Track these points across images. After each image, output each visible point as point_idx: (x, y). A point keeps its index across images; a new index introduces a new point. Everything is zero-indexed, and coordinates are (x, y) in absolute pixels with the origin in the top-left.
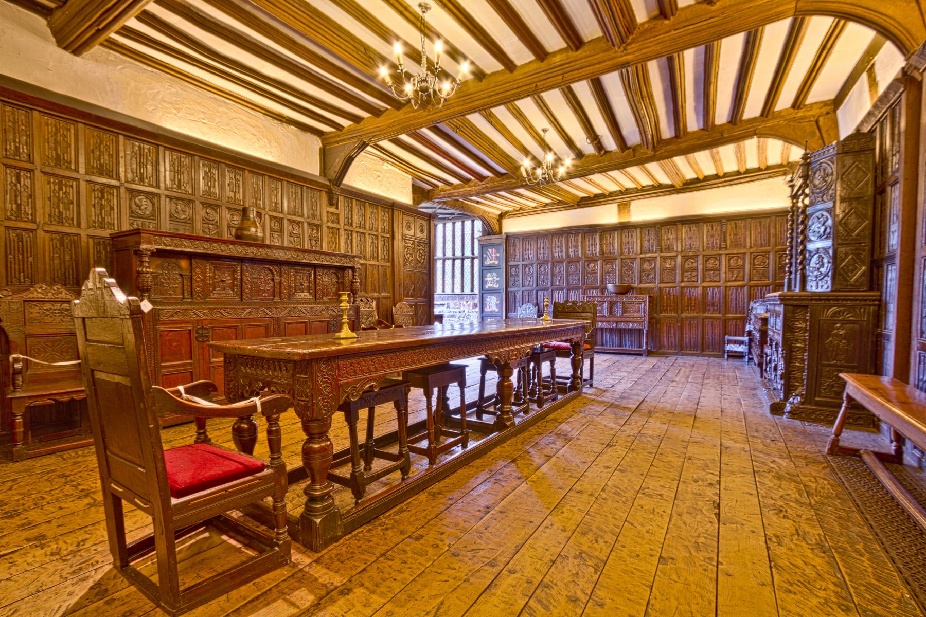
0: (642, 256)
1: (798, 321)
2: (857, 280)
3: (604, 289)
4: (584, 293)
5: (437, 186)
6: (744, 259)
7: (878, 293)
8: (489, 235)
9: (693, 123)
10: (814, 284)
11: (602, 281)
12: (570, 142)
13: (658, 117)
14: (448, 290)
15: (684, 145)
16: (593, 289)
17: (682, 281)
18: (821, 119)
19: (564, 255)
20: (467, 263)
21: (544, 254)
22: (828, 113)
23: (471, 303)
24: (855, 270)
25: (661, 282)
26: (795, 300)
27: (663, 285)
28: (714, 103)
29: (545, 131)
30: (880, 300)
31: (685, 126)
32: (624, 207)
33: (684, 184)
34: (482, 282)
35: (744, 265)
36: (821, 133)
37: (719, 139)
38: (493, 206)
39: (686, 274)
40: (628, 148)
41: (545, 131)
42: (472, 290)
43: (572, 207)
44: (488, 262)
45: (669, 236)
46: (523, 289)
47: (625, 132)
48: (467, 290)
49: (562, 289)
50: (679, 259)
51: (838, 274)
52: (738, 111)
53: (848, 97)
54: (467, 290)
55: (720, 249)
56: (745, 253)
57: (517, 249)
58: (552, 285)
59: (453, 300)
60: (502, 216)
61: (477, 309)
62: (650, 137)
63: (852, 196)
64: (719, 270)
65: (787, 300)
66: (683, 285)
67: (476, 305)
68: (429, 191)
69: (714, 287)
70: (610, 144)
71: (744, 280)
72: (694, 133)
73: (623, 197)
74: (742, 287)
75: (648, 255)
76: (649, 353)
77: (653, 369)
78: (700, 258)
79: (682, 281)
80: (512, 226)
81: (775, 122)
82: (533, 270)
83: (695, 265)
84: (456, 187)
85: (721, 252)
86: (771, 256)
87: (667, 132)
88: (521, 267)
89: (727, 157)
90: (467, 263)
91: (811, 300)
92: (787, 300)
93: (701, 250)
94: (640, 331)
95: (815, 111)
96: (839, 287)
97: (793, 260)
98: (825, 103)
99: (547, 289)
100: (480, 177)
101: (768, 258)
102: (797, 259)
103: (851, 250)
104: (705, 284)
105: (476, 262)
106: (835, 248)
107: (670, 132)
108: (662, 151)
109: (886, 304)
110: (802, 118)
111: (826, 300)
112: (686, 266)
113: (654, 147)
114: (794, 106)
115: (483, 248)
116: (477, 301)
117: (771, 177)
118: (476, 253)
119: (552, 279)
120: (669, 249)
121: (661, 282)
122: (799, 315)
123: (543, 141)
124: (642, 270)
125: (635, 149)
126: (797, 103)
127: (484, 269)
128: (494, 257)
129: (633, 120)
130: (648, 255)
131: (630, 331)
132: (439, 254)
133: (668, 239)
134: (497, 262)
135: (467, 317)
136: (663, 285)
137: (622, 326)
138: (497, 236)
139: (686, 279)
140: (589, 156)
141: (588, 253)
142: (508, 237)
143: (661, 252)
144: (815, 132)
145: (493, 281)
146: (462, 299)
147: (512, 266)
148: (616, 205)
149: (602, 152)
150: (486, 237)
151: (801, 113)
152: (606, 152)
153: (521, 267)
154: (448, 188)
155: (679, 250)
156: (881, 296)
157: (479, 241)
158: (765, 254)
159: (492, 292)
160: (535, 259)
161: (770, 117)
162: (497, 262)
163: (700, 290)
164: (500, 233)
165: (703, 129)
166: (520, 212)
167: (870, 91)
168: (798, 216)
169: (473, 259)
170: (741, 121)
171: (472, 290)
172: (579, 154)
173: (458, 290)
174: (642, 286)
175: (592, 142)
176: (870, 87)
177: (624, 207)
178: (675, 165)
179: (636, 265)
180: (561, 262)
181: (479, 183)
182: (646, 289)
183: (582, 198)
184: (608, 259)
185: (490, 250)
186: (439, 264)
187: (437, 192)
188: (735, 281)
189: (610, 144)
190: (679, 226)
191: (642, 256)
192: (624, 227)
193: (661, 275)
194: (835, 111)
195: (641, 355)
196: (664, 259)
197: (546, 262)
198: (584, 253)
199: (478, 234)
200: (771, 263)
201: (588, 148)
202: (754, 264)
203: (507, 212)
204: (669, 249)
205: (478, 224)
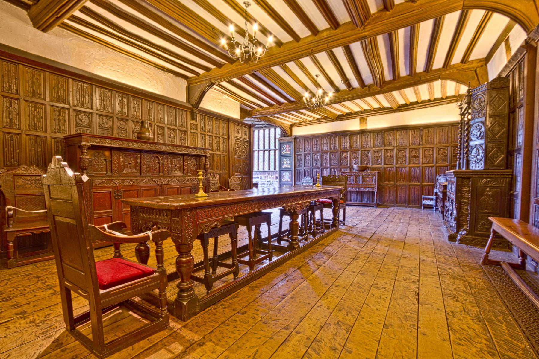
0: (374, 149)
1: (464, 187)
2: (499, 163)
3: (351, 168)
4: (340, 171)
5: (255, 108)
6: (433, 151)
7: (511, 171)
8: (285, 136)
9: (403, 71)
10: (474, 165)
11: (350, 164)
12: (332, 83)
13: (383, 68)
14: (261, 169)
15: (398, 85)
16: (345, 168)
17: (397, 164)
18: (478, 69)
19: (328, 148)
20: (272, 153)
21: (317, 148)
22: (482, 66)
23: (274, 176)
24: (498, 157)
25: (385, 164)
26: (463, 174)
27: (386, 166)
28: (416, 60)
29: (317, 76)
30: (512, 175)
31: (399, 74)
32: (363, 120)
33: (398, 107)
34: (281, 164)
35: (433, 154)
36: (478, 78)
37: (419, 81)
38: (287, 120)
39: (399, 159)
40: (366, 86)
41: (317, 76)
42: (275, 169)
43: (333, 120)
44: (284, 153)
45: (389, 137)
46: (305, 168)
47: (364, 77)
48: (272, 169)
49: (327, 168)
50: (395, 151)
51: (488, 159)
52: (429, 65)
53: (493, 57)
54: (272, 169)
55: (419, 145)
56: (433, 147)
57: (301, 145)
58: (321, 166)
59: (264, 174)
60: (292, 126)
61: (278, 180)
62: (378, 80)
63: (496, 114)
64: (419, 157)
65: (458, 174)
66: (397, 166)
67: (277, 178)
68: (250, 111)
69: (415, 167)
70: (355, 84)
71: (433, 163)
72: (404, 77)
73: (363, 115)
74: (432, 167)
75: (377, 148)
76: (378, 206)
77: (380, 215)
78: (408, 150)
79: (397, 164)
80: (298, 132)
81: (451, 71)
82: (310, 157)
83: (404, 154)
84: (265, 109)
85: (419, 147)
86: (449, 149)
87: (388, 77)
88: (303, 155)
89: (423, 92)
90: (272, 153)
91: (472, 175)
92: (458, 174)
93: (408, 145)
94: (373, 193)
95: (474, 65)
96: (488, 167)
97: (462, 151)
98: (480, 60)
99: (318, 168)
100: (280, 103)
101: (447, 150)
102: (464, 151)
103: (496, 146)
104: (410, 165)
105: (277, 152)
106: (486, 144)
107: (390, 77)
108: (385, 88)
109: (516, 177)
110: (467, 69)
111: (481, 174)
112: (400, 155)
113: (381, 85)
114: (462, 62)
115: (281, 144)
116: (277, 175)
117: (449, 103)
118: (277, 147)
119: (322, 162)
120: (389, 145)
121: (385, 164)
122: (465, 183)
123: (316, 82)
124: (374, 157)
125: (369, 86)
126: (464, 60)
127: (282, 157)
128: (287, 150)
129: (368, 70)
130: (377, 148)
131: (366, 193)
132: (256, 148)
133: (389, 139)
134: (289, 153)
135: (272, 184)
136: (386, 166)
137: (362, 189)
138: (289, 138)
139: (399, 163)
140: (343, 91)
141: (342, 147)
142: (296, 138)
143: (385, 146)
144: (474, 77)
145: (287, 163)
146: (269, 174)
147: (298, 155)
148: (358, 119)
149: (351, 89)
150: (283, 138)
151: (466, 66)
152: (353, 88)
153: (303, 155)
154: (261, 109)
155: (395, 145)
156: (513, 172)
157: (279, 140)
158: (446, 148)
159: (286, 170)
160: (311, 151)
161: (448, 68)
162: (289, 153)
163: (407, 169)
164: (291, 136)
165: (409, 75)
166: (303, 123)
167: (507, 53)
168: (465, 126)
169: (275, 151)
170: (431, 70)
171: (275, 169)
172: (337, 90)
173: (266, 169)
174: (374, 166)
175: (344, 83)
176: (507, 51)
177: (363, 120)
178: (393, 96)
179: (370, 154)
180: (327, 152)
181: (279, 106)
182: (376, 168)
183: (339, 115)
184: (354, 151)
185: (285, 146)
186: (256, 154)
187: (254, 111)
188: (428, 163)
189: (355, 84)
190: (395, 131)
191: (374, 149)
192: (363, 132)
193: (385, 160)
194: (486, 65)
195: (373, 206)
196: (387, 151)
197: (318, 152)
198: (340, 147)
199: (278, 136)
200: (449, 153)
201: (342, 86)
202: (439, 154)
203: (295, 124)
204: (389, 145)
205: (278, 131)
